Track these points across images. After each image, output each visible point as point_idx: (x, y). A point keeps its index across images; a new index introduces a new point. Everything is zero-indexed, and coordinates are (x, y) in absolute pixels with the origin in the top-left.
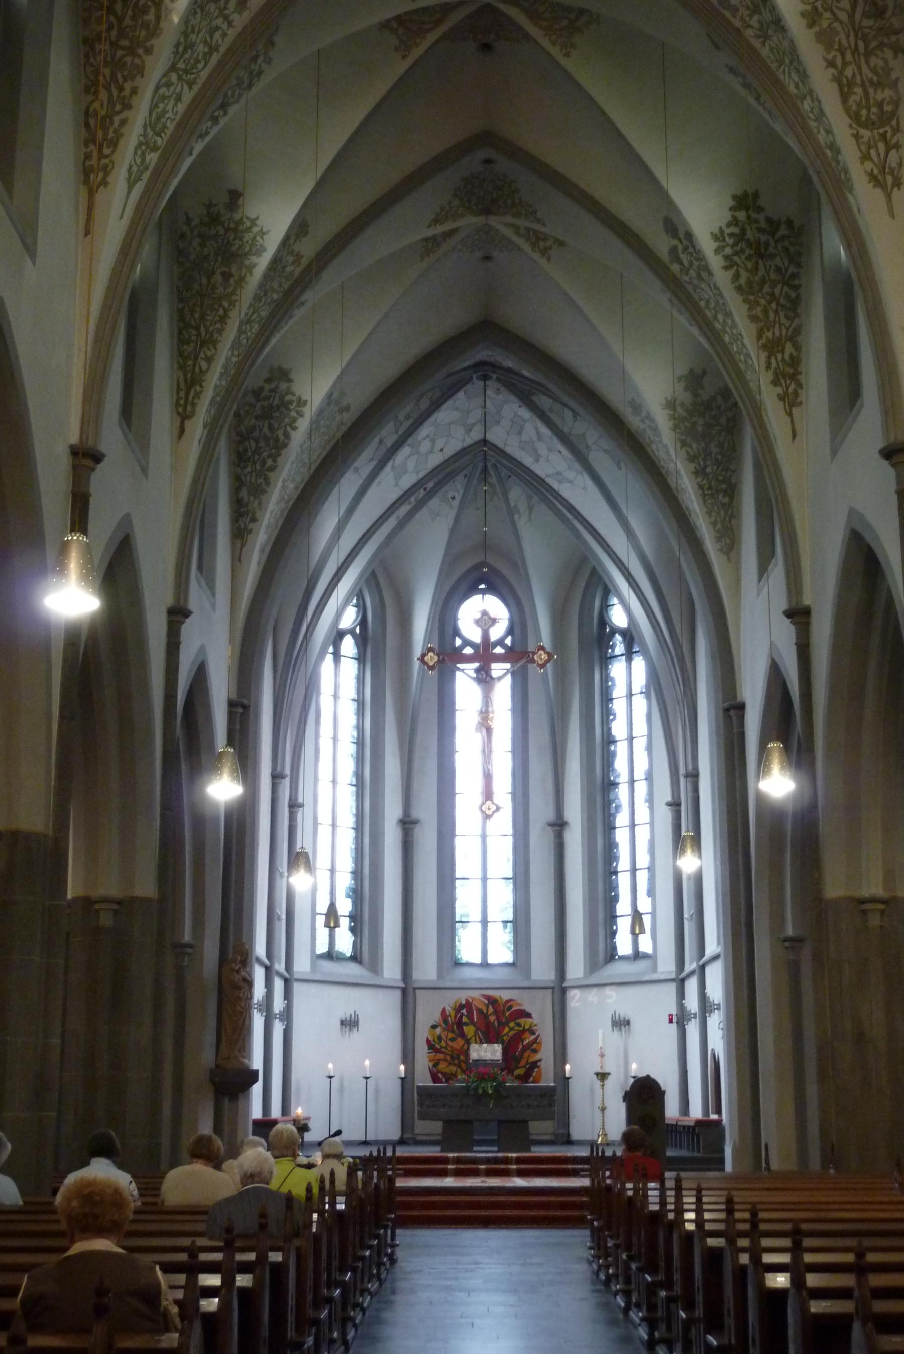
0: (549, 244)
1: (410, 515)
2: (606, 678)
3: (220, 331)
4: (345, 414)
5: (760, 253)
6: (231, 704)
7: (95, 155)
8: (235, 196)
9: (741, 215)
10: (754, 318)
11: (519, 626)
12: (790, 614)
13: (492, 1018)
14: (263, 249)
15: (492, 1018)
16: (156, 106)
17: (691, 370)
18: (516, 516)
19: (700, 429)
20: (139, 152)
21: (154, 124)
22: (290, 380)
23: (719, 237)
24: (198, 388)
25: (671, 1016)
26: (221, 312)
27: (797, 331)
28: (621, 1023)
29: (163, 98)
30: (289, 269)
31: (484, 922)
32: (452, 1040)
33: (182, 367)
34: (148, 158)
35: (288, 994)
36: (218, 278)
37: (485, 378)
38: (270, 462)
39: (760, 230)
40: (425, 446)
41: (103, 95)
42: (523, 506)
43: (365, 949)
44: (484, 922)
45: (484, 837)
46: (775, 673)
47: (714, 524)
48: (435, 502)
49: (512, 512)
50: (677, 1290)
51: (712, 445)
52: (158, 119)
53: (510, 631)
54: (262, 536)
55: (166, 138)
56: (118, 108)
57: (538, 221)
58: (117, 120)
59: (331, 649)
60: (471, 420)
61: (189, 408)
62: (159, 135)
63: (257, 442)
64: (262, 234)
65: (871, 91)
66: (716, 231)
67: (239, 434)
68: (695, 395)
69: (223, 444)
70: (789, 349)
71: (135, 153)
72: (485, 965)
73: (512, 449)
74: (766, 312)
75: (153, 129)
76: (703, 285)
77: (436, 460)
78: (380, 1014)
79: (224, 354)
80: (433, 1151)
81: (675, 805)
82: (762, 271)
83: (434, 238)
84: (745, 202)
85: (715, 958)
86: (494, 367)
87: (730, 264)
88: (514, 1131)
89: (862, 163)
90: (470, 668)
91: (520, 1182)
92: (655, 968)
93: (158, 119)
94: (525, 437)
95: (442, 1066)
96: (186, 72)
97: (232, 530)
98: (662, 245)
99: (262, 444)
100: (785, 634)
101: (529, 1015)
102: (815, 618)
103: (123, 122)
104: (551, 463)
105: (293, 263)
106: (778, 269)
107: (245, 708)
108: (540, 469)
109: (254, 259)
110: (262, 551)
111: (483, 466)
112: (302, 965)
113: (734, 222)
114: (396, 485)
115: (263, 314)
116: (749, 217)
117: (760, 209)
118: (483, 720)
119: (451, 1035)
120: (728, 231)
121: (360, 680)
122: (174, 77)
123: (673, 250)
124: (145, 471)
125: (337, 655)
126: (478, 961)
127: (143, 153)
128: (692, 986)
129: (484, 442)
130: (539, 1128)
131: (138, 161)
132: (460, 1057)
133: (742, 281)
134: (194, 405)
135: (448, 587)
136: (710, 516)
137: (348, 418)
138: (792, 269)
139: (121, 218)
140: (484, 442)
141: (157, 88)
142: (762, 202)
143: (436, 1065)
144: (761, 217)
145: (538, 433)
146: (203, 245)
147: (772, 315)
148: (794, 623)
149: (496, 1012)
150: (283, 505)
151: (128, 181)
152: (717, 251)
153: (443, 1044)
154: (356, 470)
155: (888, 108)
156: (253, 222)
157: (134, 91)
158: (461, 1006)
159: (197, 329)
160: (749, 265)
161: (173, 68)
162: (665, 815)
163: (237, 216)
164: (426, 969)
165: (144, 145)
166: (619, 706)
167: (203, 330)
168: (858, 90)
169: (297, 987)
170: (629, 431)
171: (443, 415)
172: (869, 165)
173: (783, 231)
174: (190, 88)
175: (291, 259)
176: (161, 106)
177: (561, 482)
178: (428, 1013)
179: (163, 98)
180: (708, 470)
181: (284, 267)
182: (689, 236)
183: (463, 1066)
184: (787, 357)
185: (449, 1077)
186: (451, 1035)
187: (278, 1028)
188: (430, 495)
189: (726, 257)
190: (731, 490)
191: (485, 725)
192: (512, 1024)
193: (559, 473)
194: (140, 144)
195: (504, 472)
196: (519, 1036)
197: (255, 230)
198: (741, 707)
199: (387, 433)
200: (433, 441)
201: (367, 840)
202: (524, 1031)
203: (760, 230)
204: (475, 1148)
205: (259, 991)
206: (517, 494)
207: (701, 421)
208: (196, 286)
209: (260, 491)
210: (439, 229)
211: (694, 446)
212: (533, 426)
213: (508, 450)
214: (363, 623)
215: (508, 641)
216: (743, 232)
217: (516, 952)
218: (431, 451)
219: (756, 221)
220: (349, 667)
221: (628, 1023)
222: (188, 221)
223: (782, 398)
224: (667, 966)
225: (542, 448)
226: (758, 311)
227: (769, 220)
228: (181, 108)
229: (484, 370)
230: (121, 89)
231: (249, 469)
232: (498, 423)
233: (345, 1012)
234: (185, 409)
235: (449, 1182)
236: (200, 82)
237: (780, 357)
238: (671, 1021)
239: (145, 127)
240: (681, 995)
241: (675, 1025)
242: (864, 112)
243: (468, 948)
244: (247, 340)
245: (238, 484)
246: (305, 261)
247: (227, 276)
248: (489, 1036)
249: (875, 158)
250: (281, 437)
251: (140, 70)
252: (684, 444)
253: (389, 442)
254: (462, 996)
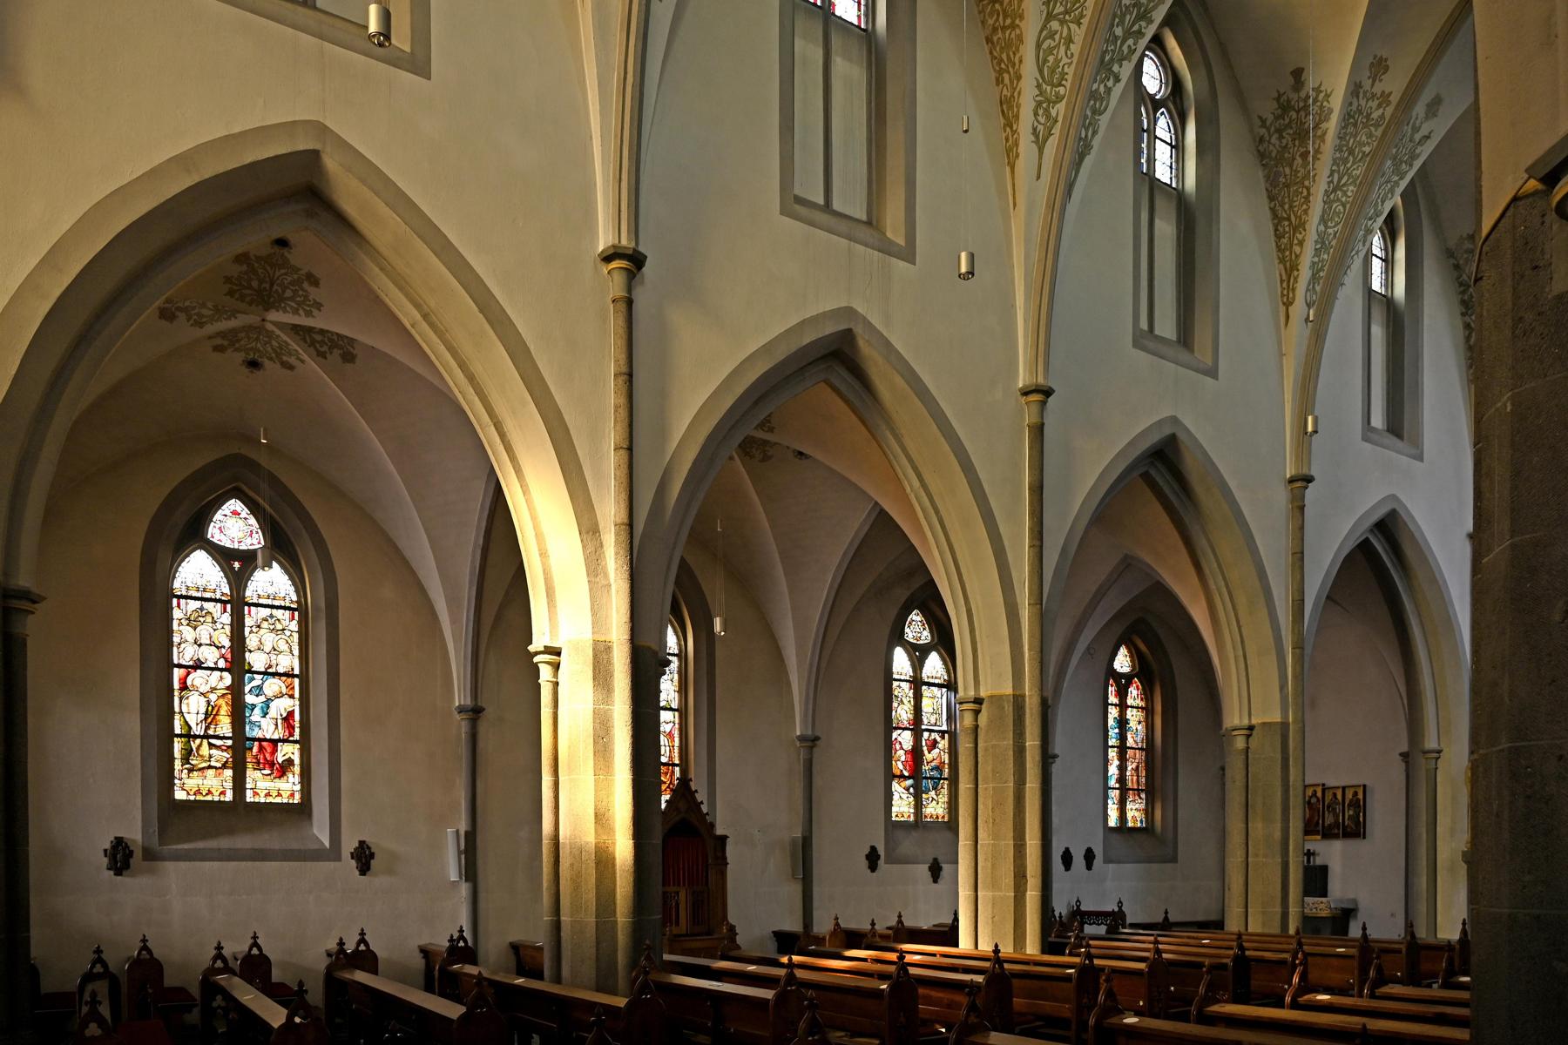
3: (1306, 212)
8: (1298, 74)
14: (1331, 111)
16: (1046, 61)
20: (1041, 112)
21: (1049, 76)
29: (1050, 50)
30: (1375, 115)
33: (1282, 260)
36: (1299, 161)
55: (1068, 85)
62: (1060, 85)
64: (1328, 96)
67: (1461, 284)
71: (1036, 114)
93: (1053, 72)
96: (1067, 12)
105: (1379, 106)
109: (1324, 126)
122: (1055, 25)
127: (1047, 111)
131: (1042, 120)
139: (1038, 177)
141: (1038, 46)
146: (1281, 137)
151: (1037, 142)
156: (1318, 90)
159: (1289, 219)
161: (1050, 17)
163: (1303, 94)
165: (1043, 104)
174: (1079, 24)
175: (1374, 104)
176: (1051, 58)
179: (1050, 50)
181: (1368, 116)
194: (1039, 104)
197: (1321, 96)
208: (1282, 180)
222: (1263, 121)
228: (1075, 49)
236: (1088, 13)
239: (1039, 86)
244: (1344, 205)
247: (1305, 155)
251: (1020, 39)
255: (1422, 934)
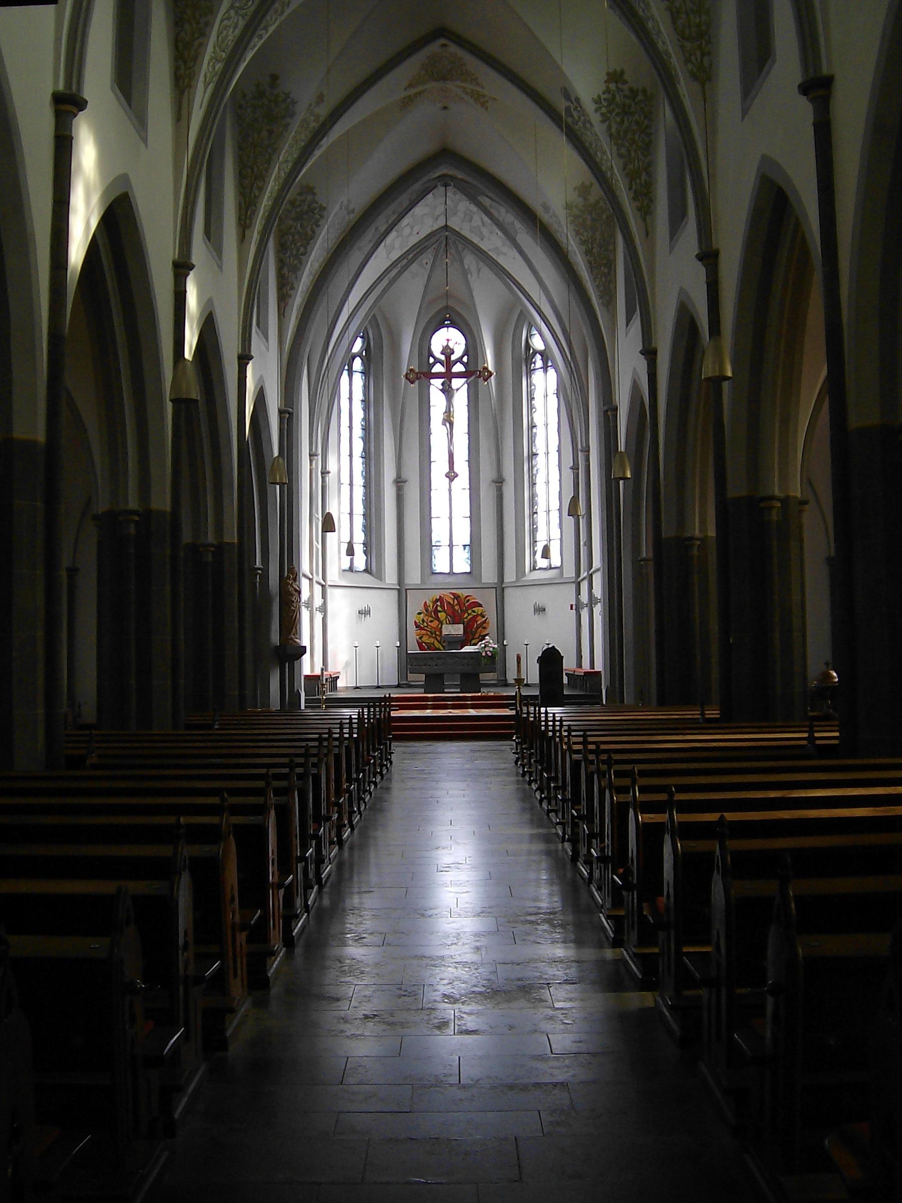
0: (486, 99)
1: (400, 273)
2: (530, 384)
4: (352, 216)
5: (625, 112)
6: (281, 412)
7: (182, 67)
8: (274, 78)
9: (612, 86)
10: (620, 156)
11: (473, 349)
12: (701, 258)
13: (457, 608)
15: (457, 608)
17: (583, 184)
18: (469, 276)
19: (589, 222)
22: (315, 194)
23: (597, 101)
24: (254, 208)
25: (572, 606)
26: (267, 157)
27: (650, 164)
28: (540, 610)
29: (226, 28)
31: (451, 546)
32: (431, 621)
34: (217, 68)
35: (324, 596)
36: (265, 134)
37: (446, 185)
38: (302, 250)
39: (626, 97)
40: (407, 231)
41: (187, 27)
42: (473, 268)
43: (374, 564)
44: (451, 546)
45: (450, 490)
46: (635, 387)
47: (598, 287)
48: (414, 267)
49: (465, 273)
50: (560, 784)
51: (598, 233)
52: (223, 42)
53: (466, 353)
54: (298, 300)
56: (196, 35)
57: (478, 84)
58: (196, 43)
59: (346, 367)
60: (437, 213)
61: (248, 221)
63: (293, 236)
64: (294, 103)
65: (692, 16)
66: (596, 97)
68: (585, 199)
69: (271, 245)
70: (644, 176)
72: (451, 573)
73: (466, 233)
74: (629, 151)
75: (220, 48)
76: (588, 133)
77: (414, 240)
78: (384, 606)
79: (272, 186)
80: (419, 693)
81: (575, 468)
82: (626, 124)
83: (409, 97)
84: (615, 77)
85: (598, 570)
86: (452, 178)
87: (605, 119)
88: (470, 680)
89: (686, 64)
90: (437, 383)
91: (472, 712)
92: (562, 573)
93: (223, 42)
94: (474, 224)
95: (425, 639)
97: (278, 297)
98: (561, 105)
99: (297, 237)
100: (642, 365)
101: (480, 606)
102: (723, 257)
103: (201, 45)
104: (492, 241)
106: (637, 123)
107: (291, 414)
108: (484, 246)
110: (298, 310)
111: (445, 240)
112: (333, 576)
113: (607, 91)
114: (388, 257)
115: (295, 156)
116: (617, 87)
117: (625, 82)
118: (449, 415)
119: (430, 619)
120: (603, 97)
121: (366, 388)
122: (232, 13)
123: (568, 109)
124: (220, 267)
125: (351, 373)
126: (448, 571)
128: (584, 586)
129: (446, 227)
130: (485, 677)
132: (436, 633)
133: (613, 130)
134: (251, 220)
135: (422, 325)
136: (595, 281)
137: (353, 218)
138: (646, 122)
140: (446, 227)
141: (222, 21)
142: (626, 77)
143: (420, 638)
144: (625, 87)
145: (483, 222)
147: (633, 154)
148: (811, 101)
149: (458, 604)
150: (311, 278)
152: (596, 110)
153: (425, 624)
154: (360, 249)
155: (704, 28)
156: (287, 96)
157: (207, 24)
158: (437, 600)
160: (618, 120)
161: (232, 7)
162: (569, 475)
164: (414, 577)
166: (538, 402)
167: (255, 170)
168: (683, 16)
169: (329, 591)
170: (541, 222)
171: (418, 210)
172: (690, 66)
173: (640, 97)
174: (243, 18)
175: (312, 118)
176: (225, 32)
177: (498, 254)
178: (415, 606)
179: (226, 28)
180: (595, 250)
182: (577, 100)
183: (438, 638)
184: (643, 181)
185: (430, 646)
186: (430, 619)
187: (318, 617)
188: (411, 262)
189: (603, 115)
190: (611, 265)
191: (448, 420)
192: (470, 611)
193: (497, 248)
195: (460, 247)
196: (474, 619)
197: (289, 100)
198: (616, 409)
199: (381, 223)
200: (412, 228)
201: (373, 494)
202: (478, 615)
203: (626, 97)
204: (446, 690)
205: (305, 595)
206: (470, 260)
207: (589, 217)
209: (296, 269)
210: (413, 91)
211: (585, 234)
212: (479, 217)
213: (462, 233)
214: (367, 347)
215: (465, 359)
216: (614, 97)
217: (471, 566)
218: (411, 234)
219: (622, 90)
220: (358, 380)
221: (544, 610)
222: (244, 96)
223: (639, 209)
224: (569, 572)
225: (485, 231)
226: (623, 151)
227: (631, 90)
228: (237, 32)
229: (446, 181)
230: (198, 23)
231: (288, 254)
232: (455, 214)
233: (362, 606)
234: (245, 222)
235: (428, 713)
237: (638, 181)
238: (572, 609)
239: (214, 47)
240: (578, 592)
241: (574, 611)
242: (687, 31)
243: (440, 563)
245: (281, 264)
246: (322, 119)
247: (270, 132)
248: (455, 619)
249: (694, 62)
250: (309, 232)
252: (578, 233)
253: (383, 229)
254: (436, 594)
255: (523, 676)
